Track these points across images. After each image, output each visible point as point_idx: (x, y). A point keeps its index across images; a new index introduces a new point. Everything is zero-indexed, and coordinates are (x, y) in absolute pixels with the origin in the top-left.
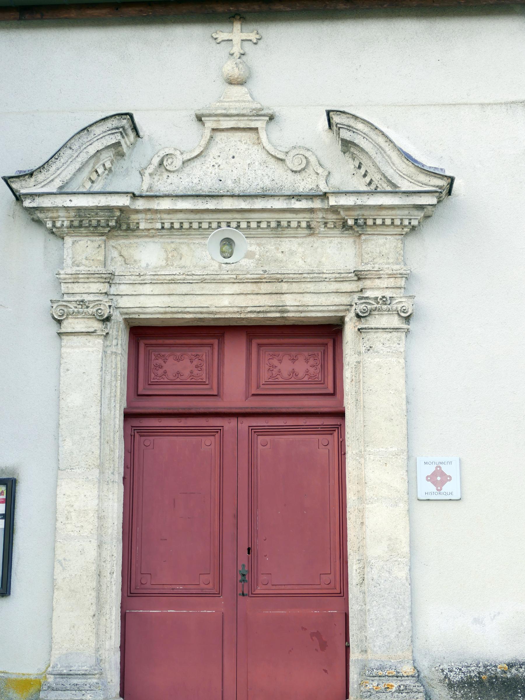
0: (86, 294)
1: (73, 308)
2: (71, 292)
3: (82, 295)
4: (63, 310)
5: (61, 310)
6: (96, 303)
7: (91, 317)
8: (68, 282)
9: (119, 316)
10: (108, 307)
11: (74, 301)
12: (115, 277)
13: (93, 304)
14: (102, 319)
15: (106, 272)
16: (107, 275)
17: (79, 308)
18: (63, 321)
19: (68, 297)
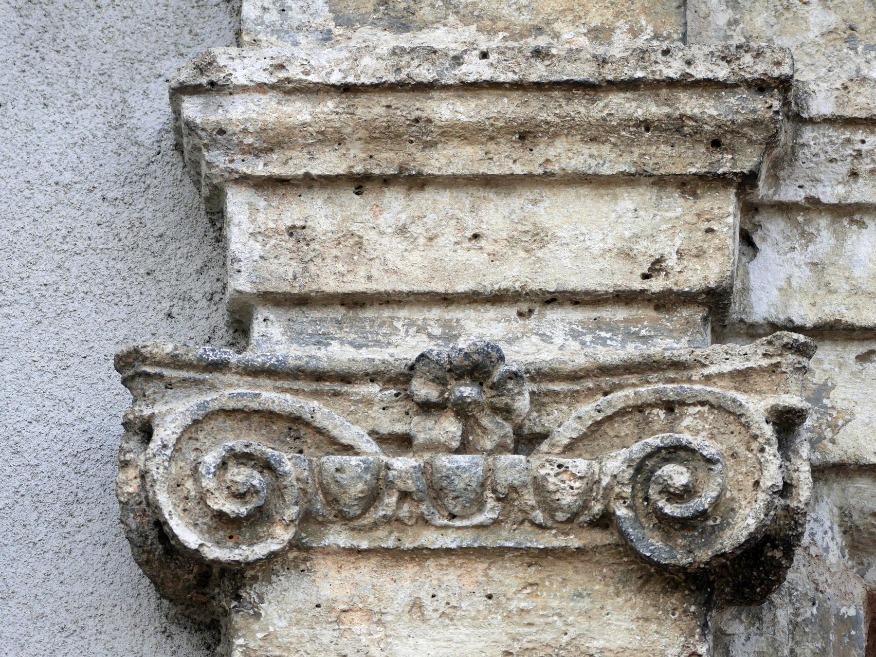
0: (491, 313)
1: (371, 447)
2: (331, 285)
3: (454, 314)
4: (267, 466)
5: (244, 458)
6: (620, 398)
7: (574, 541)
8: (310, 182)
9: (833, 557)
10: (768, 430)
11: (372, 377)
12: (808, 134)
13: (588, 409)
14: (704, 555)
15: (722, 72)
16: (732, 100)
17: (435, 447)
18: (249, 594)
19: (297, 337)
